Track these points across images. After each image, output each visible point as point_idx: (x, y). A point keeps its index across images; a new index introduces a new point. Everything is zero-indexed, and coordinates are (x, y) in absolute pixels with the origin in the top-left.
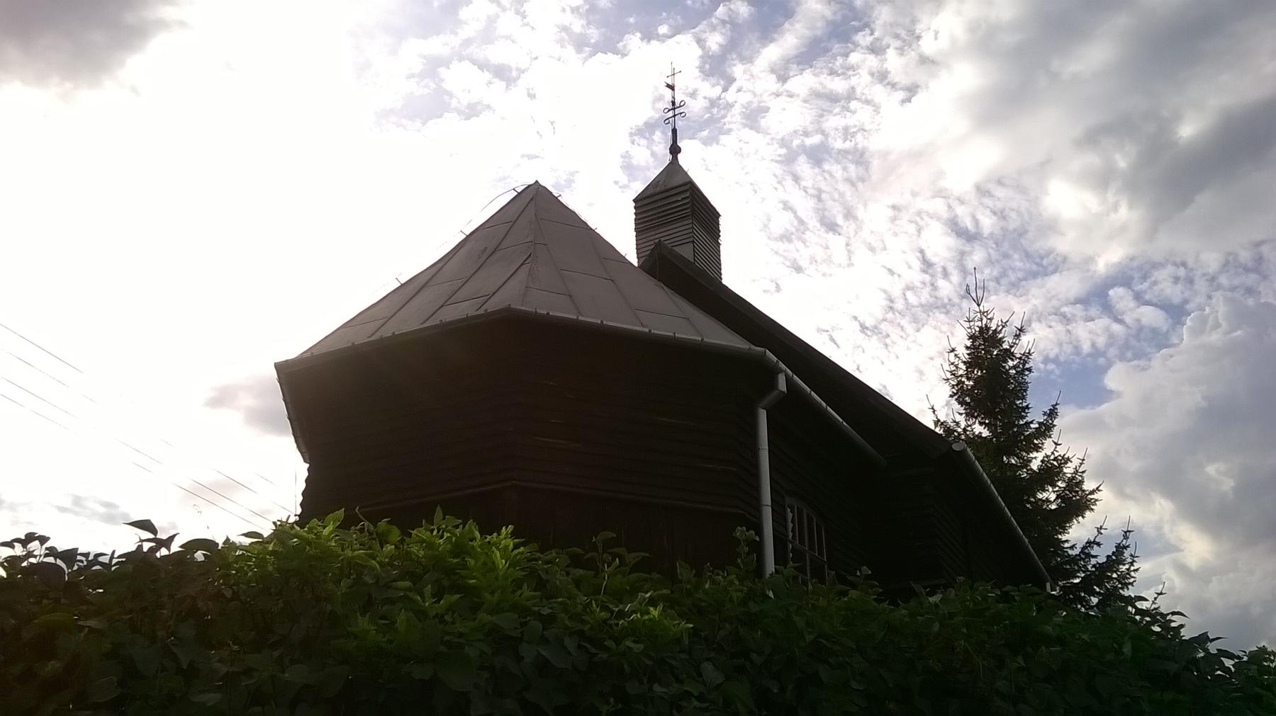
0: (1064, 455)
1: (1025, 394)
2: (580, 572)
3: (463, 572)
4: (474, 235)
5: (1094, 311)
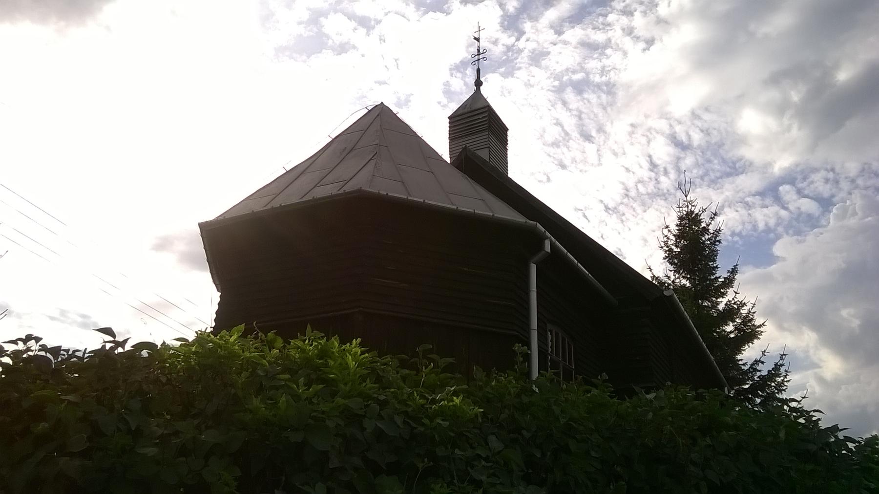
0: (742, 301)
5: (768, 201)
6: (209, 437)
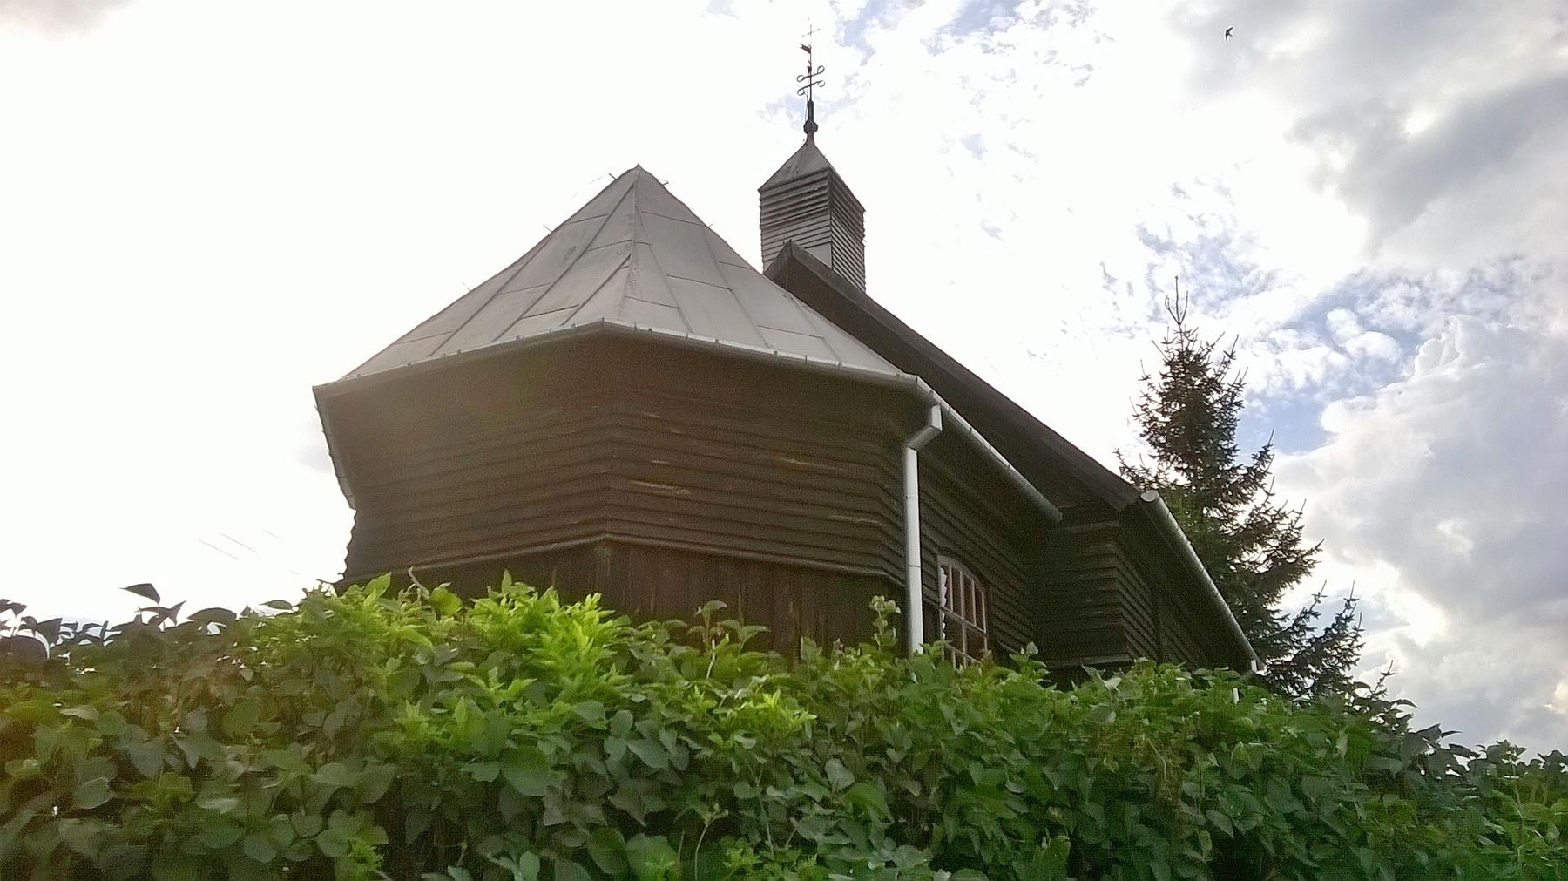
0: (1280, 509)
1: (1231, 433)
2: (680, 650)
3: (537, 651)
4: (559, 231)
5: (1309, 338)
6: (332, 776)
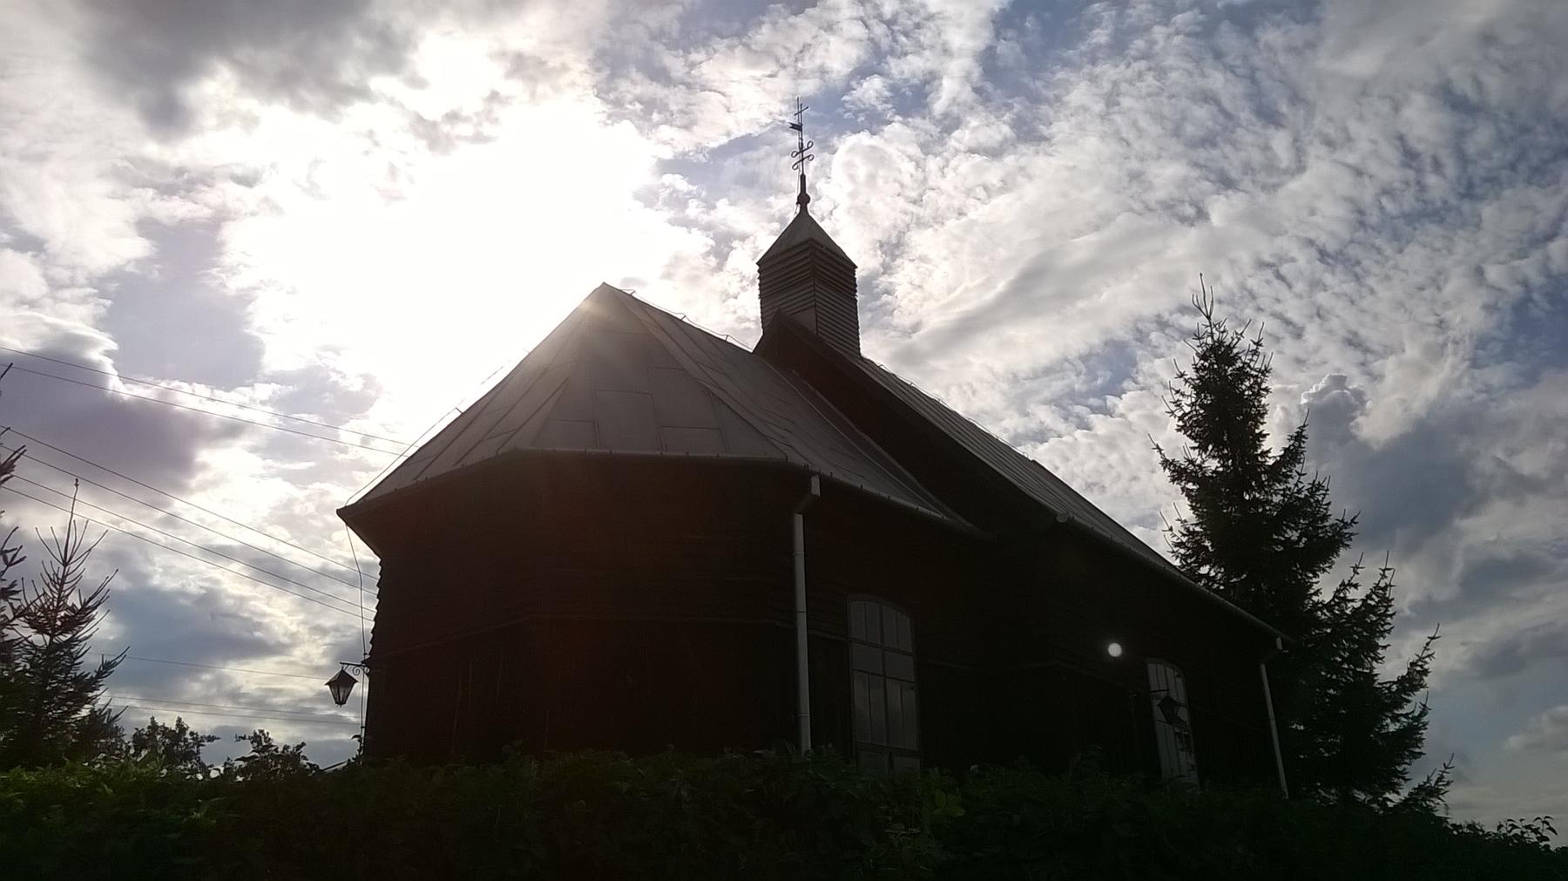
0: (1314, 481)
